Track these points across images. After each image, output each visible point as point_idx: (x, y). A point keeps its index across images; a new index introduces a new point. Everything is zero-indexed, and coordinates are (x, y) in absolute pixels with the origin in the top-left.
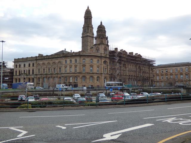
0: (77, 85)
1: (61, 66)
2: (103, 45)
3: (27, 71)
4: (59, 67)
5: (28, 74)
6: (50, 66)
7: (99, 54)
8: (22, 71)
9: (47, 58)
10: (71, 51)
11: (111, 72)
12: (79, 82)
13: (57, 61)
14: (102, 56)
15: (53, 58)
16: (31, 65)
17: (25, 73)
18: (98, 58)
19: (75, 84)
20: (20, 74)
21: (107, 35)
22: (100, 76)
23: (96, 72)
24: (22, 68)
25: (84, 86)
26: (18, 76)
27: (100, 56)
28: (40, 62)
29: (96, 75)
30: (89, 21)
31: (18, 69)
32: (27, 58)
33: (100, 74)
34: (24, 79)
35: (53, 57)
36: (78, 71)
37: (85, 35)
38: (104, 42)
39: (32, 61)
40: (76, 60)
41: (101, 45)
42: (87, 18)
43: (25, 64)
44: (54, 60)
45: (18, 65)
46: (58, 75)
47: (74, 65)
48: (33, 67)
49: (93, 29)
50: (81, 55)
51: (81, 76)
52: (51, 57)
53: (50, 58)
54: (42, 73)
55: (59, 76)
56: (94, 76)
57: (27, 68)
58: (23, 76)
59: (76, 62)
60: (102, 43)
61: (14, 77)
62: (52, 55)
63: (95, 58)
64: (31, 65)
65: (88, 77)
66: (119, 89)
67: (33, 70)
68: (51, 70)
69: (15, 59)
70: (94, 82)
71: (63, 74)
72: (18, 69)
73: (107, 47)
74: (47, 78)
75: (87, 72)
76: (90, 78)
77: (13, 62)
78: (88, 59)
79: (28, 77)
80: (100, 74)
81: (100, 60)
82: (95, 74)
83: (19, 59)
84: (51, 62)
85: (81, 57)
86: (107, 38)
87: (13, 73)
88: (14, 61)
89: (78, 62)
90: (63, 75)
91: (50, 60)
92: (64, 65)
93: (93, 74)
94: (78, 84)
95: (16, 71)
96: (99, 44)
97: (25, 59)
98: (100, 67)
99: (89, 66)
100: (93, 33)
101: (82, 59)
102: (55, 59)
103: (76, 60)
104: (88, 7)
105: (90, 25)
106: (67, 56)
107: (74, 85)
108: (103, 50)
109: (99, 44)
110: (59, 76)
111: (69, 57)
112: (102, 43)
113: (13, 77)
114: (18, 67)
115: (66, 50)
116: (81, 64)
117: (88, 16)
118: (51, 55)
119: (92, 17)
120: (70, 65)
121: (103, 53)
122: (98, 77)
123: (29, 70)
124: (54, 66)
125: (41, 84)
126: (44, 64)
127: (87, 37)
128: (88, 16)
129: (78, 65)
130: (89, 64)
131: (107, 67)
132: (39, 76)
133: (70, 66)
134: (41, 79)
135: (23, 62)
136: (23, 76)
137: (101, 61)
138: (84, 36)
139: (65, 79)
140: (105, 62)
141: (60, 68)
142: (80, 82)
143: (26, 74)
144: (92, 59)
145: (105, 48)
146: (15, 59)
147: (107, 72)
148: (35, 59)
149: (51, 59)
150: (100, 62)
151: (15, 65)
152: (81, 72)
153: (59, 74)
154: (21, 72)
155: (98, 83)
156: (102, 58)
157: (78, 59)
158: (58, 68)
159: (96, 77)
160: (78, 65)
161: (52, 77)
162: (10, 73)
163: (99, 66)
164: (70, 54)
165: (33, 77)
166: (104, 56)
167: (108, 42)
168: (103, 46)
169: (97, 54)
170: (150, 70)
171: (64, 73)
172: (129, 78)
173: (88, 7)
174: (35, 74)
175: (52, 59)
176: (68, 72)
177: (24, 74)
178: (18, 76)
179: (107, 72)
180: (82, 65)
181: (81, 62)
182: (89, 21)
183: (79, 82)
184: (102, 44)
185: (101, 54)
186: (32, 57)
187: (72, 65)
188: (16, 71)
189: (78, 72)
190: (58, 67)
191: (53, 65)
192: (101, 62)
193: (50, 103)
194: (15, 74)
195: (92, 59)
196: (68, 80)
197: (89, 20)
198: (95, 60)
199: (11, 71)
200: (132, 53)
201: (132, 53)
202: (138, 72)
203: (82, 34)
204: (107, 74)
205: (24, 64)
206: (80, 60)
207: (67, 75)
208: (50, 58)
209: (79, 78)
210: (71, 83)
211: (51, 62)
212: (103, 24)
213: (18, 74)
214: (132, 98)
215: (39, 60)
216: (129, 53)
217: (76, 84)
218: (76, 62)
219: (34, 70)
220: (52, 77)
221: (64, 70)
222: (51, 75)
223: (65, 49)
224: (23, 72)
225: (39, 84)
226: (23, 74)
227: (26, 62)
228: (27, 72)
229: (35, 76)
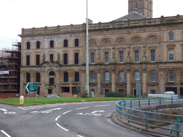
1: (156, 45)
3: (59, 56)
5: (62, 63)
9: (116, 26)
13: (144, 35)
15: (135, 27)
16: (71, 43)
17: (55, 59)
20: (41, 61)
24: (45, 50)
26: (33, 67)
31: (33, 52)
32: (59, 26)
34: (52, 73)
35: (131, 25)
39: (73, 35)
43: (54, 40)
44: (134, 33)
45: (33, 42)
46: (149, 66)
48: (78, 49)
52: (126, 26)
53: (125, 28)
54: (102, 61)
55: (150, 67)
57: (59, 50)
58: (47, 68)
61: (22, 69)
62: (113, 22)
64: (71, 43)
67: (76, 55)
68: (127, 55)
69: (23, 30)
71: (165, 63)
72: (33, 52)
77: (19, 35)
79: (64, 69)
84: (113, 37)
87: (19, 61)
90: (162, 66)
91: (123, 31)
92: (165, 44)
95: (28, 57)
97: (55, 30)
102: (138, 29)
106: (175, 23)
110: (150, 67)
113: (19, 69)
114: (33, 46)
118: (110, 23)
123: (66, 56)
124: (134, 46)
125: (99, 86)
126: (106, 41)
135: (46, 37)
136: (47, 68)
139: (167, 75)
140: (80, 45)
141: (153, 51)
143: (57, 62)
146: (23, 30)
148: (81, 29)
149: (127, 30)
153: (151, 64)
154: (41, 58)
158: (132, 51)
161: (146, 70)
162: (10, 59)
165: (76, 70)
171: (165, 60)
175: (130, 30)
177: (51, 64)
178: (33, 67)
186: (72, 25)
188: (28, 57)
190: (147, 48)
193: (136, 128)
194: (24, 62)
199: (12, 55)
205: (50, 40)
208: (125, 28)
211: (128, 37)
213: (33, 62)
217: (78, 86)
221: (165, 55)
222: (129, 65)
224: (48, 59)
226: (47, 62)
227: (56, 36)
228: (58, 59)
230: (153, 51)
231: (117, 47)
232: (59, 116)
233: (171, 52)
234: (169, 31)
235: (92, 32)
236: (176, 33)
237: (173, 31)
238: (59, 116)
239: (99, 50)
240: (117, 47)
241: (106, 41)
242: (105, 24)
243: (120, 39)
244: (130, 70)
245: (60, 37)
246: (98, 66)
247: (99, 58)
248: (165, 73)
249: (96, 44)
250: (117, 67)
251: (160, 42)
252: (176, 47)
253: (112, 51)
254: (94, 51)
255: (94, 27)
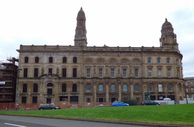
5: (61, 76)
8: (43, 70)
34: (50, 84)
37: (80, 38)
42: (80, 19)
66: (70, 92)
69: (21, 46)
79: (63, 81)
83: (33, 46)
84: (95, 57)
90: (145, 80)
102: (125, 54)
104: (81, 8)
111: (156, 54)
113: (16, 81)
138: (78, 39)
143: (56, 75)
146: (21, 46)
149: (117, 54)
151: (24, 56)
165: (74, 82)
173: (81, 8)
174: (78, 75)
197: (82, 22)
205: (49, 56)
209: (176, 85)
210: (160, 93)
212: (168, 21)
214: (49, 97)
219: (78, 70)
224: (46, 72)
226: (46, 75)
227: (55, 54)
229: (81, 81)
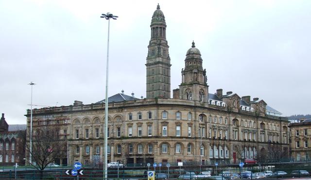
0: (153, 158)
1: (120, 123)
2: (199, 85)
4: (95, 126)
6: (100, 125)
7: (192, 102)
10: (142, 97)
11: (213, 136)
12: (157, 153)
14: (197, 105)
18: (189, 109)
19: (137, 157)
21: (204, 66)
22: (194, 143)
23: (186, 136)
25: (180, 161)
27: (193, 105)
28: (79, 117)
29: (188, 141)
30: (161, 34)
33: (194, 138)
36: (154, 134)
38: (199, 80)
40: (150, 114)
41: (194, 85)
47: (147, 123)
49: (169, 49)
50: (160, 105)
51: (159, 143)
54: (83, 136)
56: (183, 143)
59: (150, 117)
60: (196, 82)
62: (92, 105)
63: (185, 110)
65: (172, 144)
68: (101, 132)
70: (183, 154)
73: (204, 89)
74: (92, 146)
75: (170, 135)
76: (175, 147)
78: (172, 111)
80: (194, 138)
81: (193, 113)
82: (184, 139)
85: (160, 108)
86: (204, 72)
88: (26, 114)
89: (153, 118)
90: (124, 141)
93: (182, 139)
94: (154, 156)
96: (191, 84)
98: (193, 125)
99: (175, 125)
100: (169, 56)
101: (160, 111)
103: (150, 114)
104: (158, 7)
105: (163, 42)
107: (137, 159)
108: (198, 95)
109: (191, 84)
112: (195, 82)
115: (125, 93)
116: (160, 120)
117: (158, 25)
119: (166, 26)
120: (137, 122)
121: (198, 99)
122: (190, 144)
125: (81, 157)
126: (87, 120)
127: (158, 65)
128: (158, 25)
129: (155, 122)
130: (175, 121)
131: (206, 126)
132: (77, 142)
133: (137, 124)
134: (81, 149)
137: (195, 114)
138: (152, 62)
139: (128, 148)
141: (119, 129)
142: (158, 154)
144: (165, 111)
145: (202, 91)
147: (206, 136)
150: (193, 115)
152: (160, 135)
153: (85, 140)
155: (191, 155)
156: (197, 109)
157: (154, 112)
158: (94, 129)
159: (186, 144)
160: (155, 122)
163: (192, 124)
164: (138, 101)
166: (199, 105)
167: (206, 79)
168: (198, 88)
169: (190, 103)
170: (282, 128)
172: (245, 146)
173: (158, 7)
176: (144, 134)
179: (206, 136)
180: (162, 123)
181: (160, 118)
182: (161, 34)
183: (157, 153)
184: (196, 83)
185: (195, 101)
187: (141, 122)
189: (154, 135)
191: (94, 122)
192: (195, 117)
195: (165, 111)
196: (135, 150)
198: (185, 114)
200: (249, 97)
201: (249, 97)
202: (259, 134)
203: (148, 59)
204: (206, 138)
206: (158, 114)
207: (142, 140)
209: (155, 147)
215: (79, 113)
216: (243, 97)
218: (150, 117)
220: (92, 144)
223: (123, 91)
225: (78, 156)
230: (119, 129)
231: (94, 125)
232: (286, 173)
233: (140, 129)
234: (138, 112)
235: (112, 110)
236: (134, 114)
237: (151, 111)
238: (286, 173)
239: (91, 126)
240: (94, 125)
241: (87, 120)
242: (246, 98)
243: (96, 119)
244: (92, 144)
245: (54, 116)
246: (81, 141)
247: (92, 134)
248: (127, 147)
249: (79, 122)
250: (93, 141)
251: (123, 121)
252: (133, 125)
253: (90, 128)
254: (78, 129)
255: (143, 102)
